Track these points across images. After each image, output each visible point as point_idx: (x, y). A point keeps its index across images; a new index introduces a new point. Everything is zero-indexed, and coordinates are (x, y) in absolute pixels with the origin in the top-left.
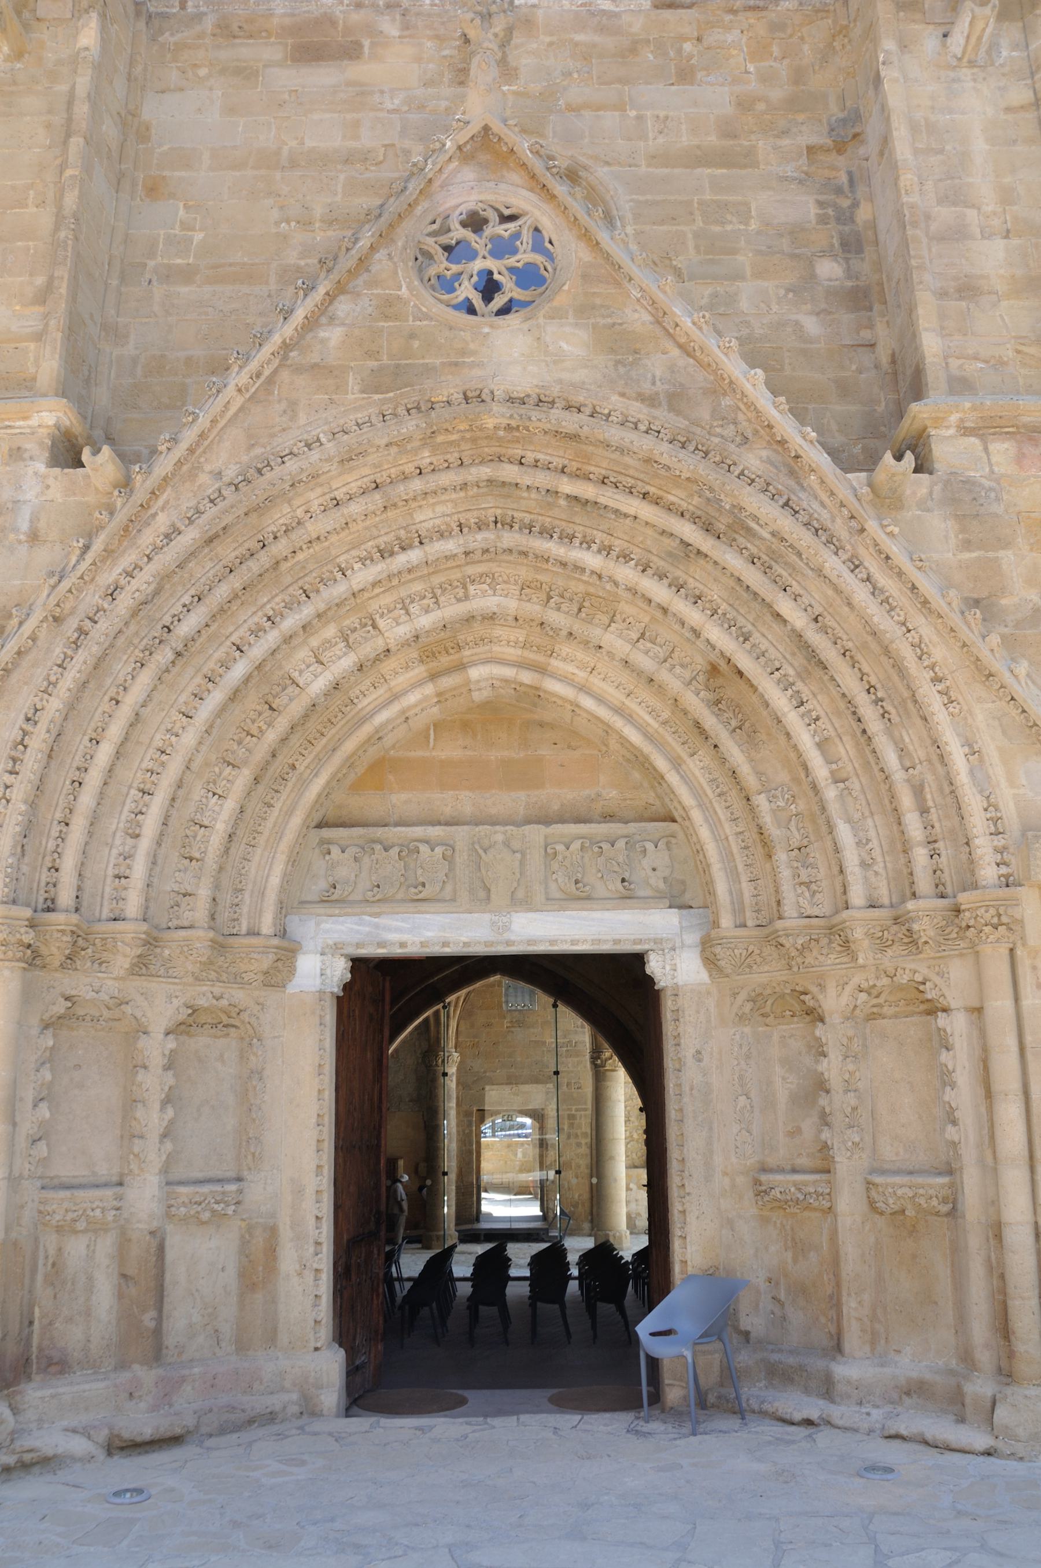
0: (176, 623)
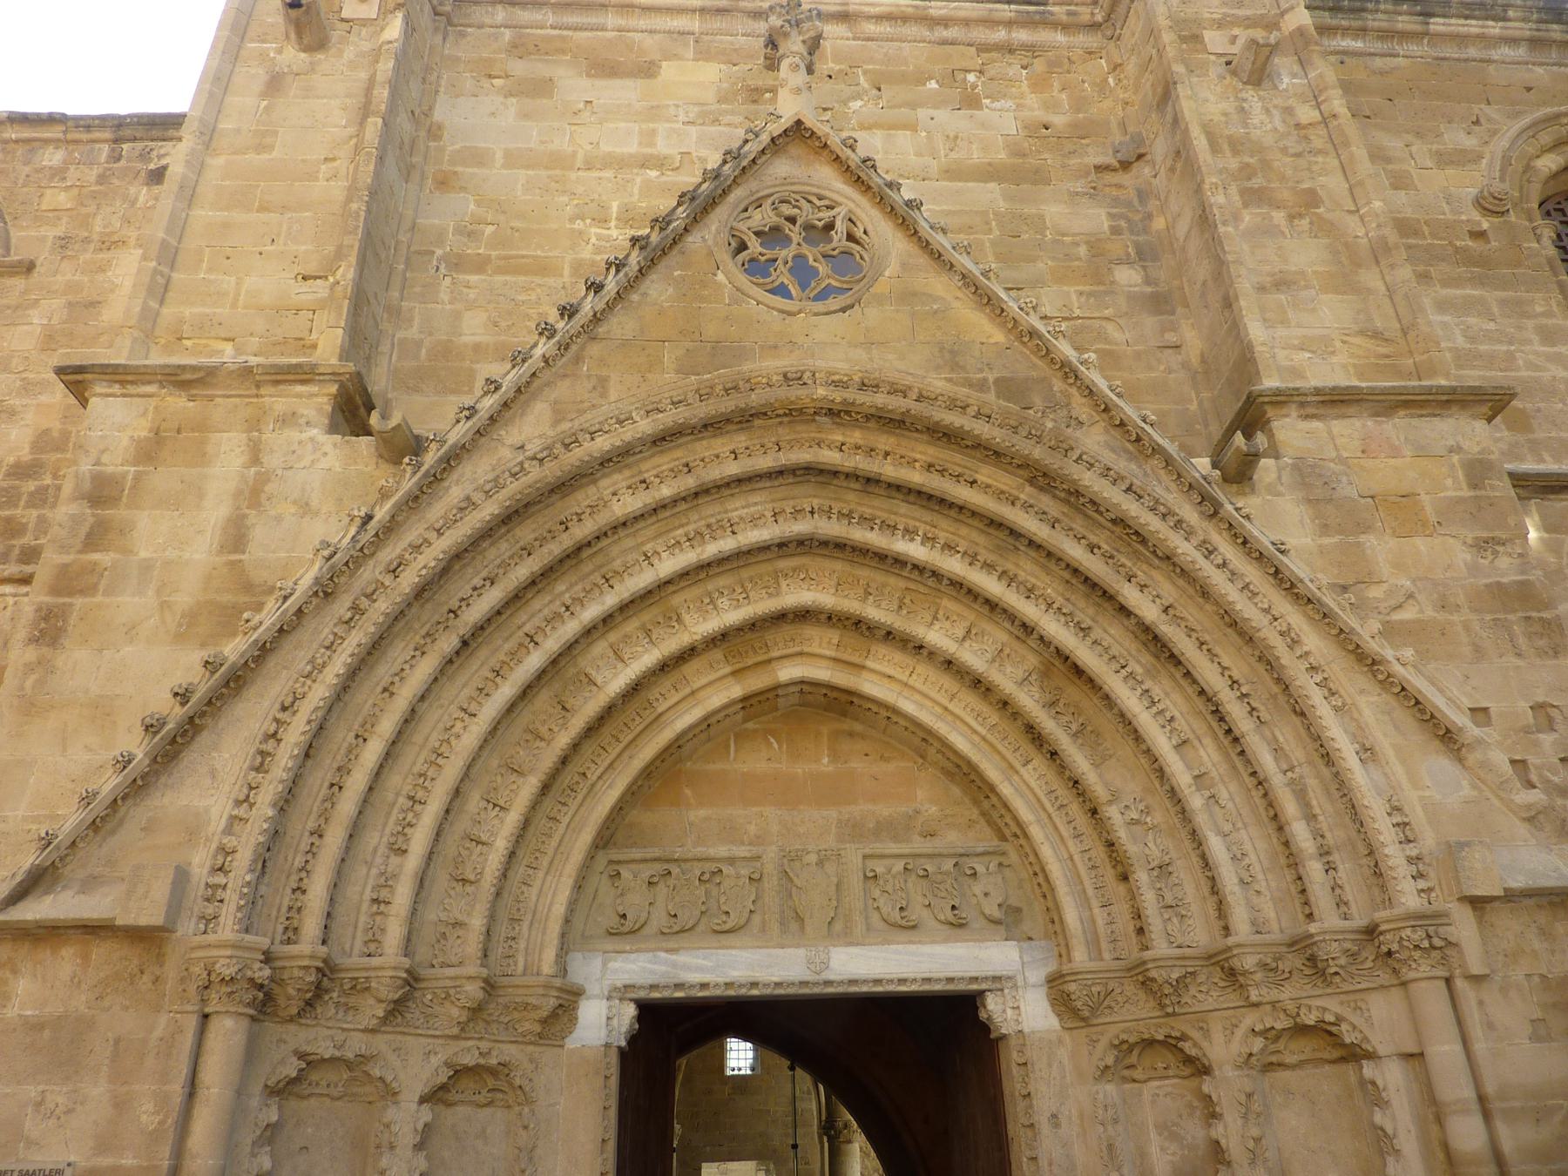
0: (464, 608)
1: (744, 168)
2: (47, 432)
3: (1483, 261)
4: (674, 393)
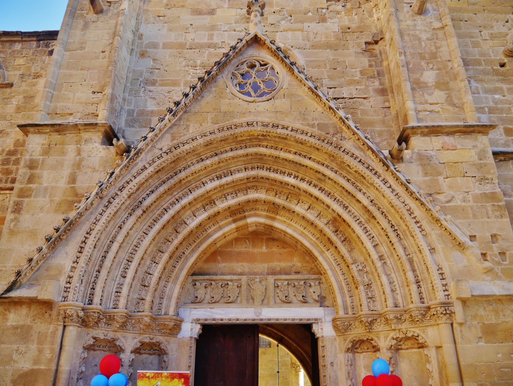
1: (237, 53)
2: (18, 140)
3: (503, 74)
4: (210, 130)
